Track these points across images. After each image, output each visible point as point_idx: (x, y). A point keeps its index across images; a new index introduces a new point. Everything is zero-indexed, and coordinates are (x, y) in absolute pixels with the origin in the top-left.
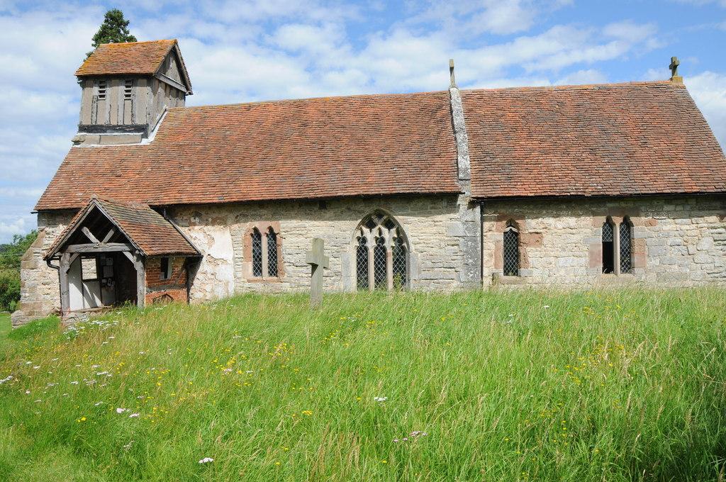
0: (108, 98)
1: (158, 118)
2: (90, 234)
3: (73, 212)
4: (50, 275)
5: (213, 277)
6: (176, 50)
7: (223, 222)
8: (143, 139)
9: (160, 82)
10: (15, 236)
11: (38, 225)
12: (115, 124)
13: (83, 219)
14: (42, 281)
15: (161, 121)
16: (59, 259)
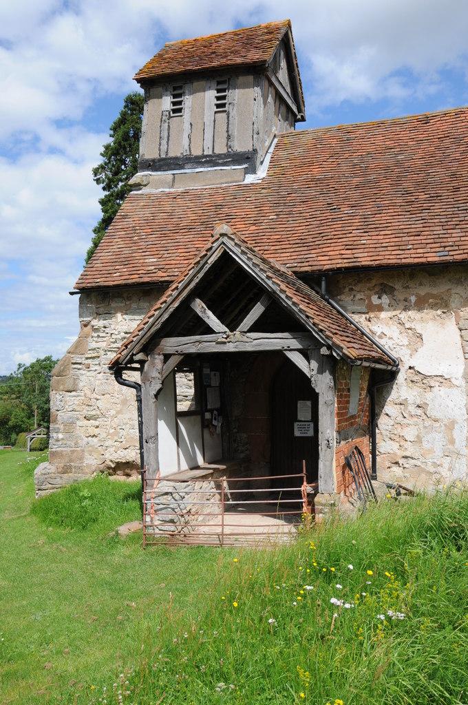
0: (187, 113)
1: (267, 144)
2: (210, 313)
3: (149, 291)
4: (99, 403)
5: (419, 412)
6: (288, 40)
7: (442, 304)
8: (247, 176)
9: (271, 84)
10: (20, 365)
11: (80, 316)
12: (199, 153)
13: (196, 280)
14: (85, 413)
15: (271, 150)
16: (141, 370)
